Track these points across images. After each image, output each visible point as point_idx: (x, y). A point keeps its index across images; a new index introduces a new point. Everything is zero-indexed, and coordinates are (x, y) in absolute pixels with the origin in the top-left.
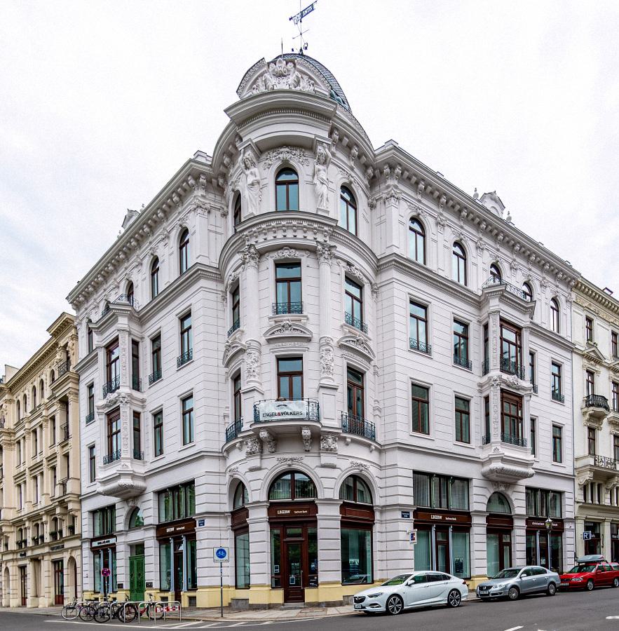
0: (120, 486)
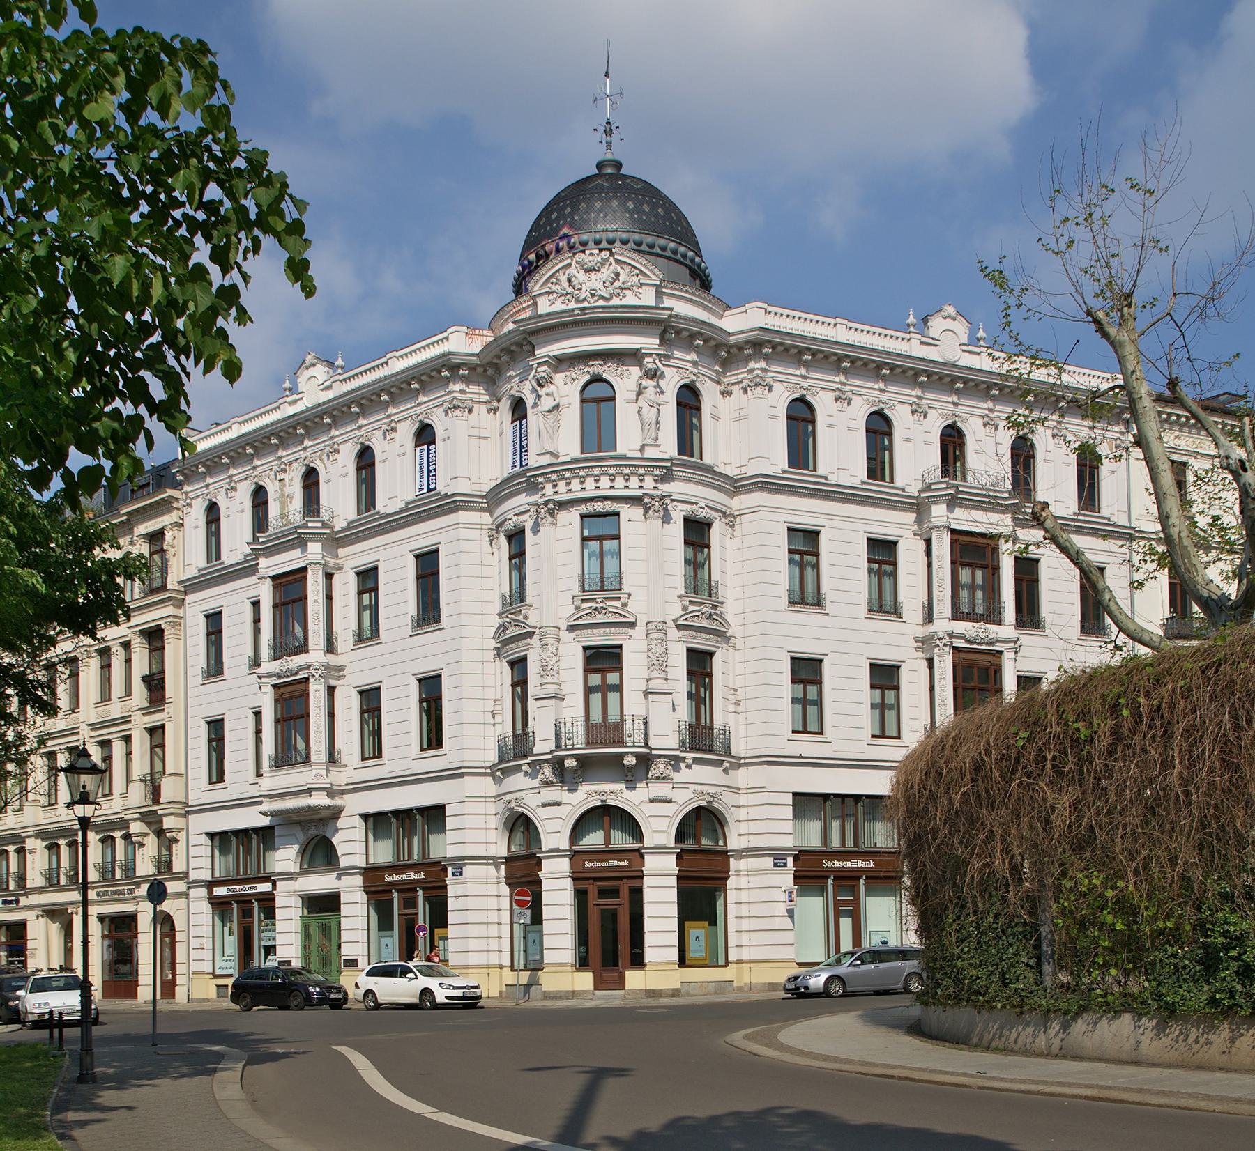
0: (310, 809)
